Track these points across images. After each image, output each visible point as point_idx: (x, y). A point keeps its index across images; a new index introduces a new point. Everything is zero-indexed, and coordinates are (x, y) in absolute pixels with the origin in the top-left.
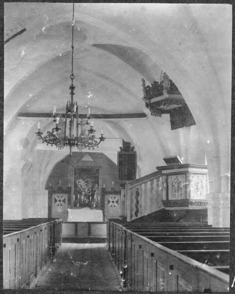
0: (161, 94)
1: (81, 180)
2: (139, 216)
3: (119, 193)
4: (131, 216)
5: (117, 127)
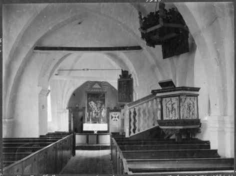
0: (157, 23)
1: (92, 102)
2: (137, 132)
3: (120, 111)
4: (130, 133)
5: (115, 57)
